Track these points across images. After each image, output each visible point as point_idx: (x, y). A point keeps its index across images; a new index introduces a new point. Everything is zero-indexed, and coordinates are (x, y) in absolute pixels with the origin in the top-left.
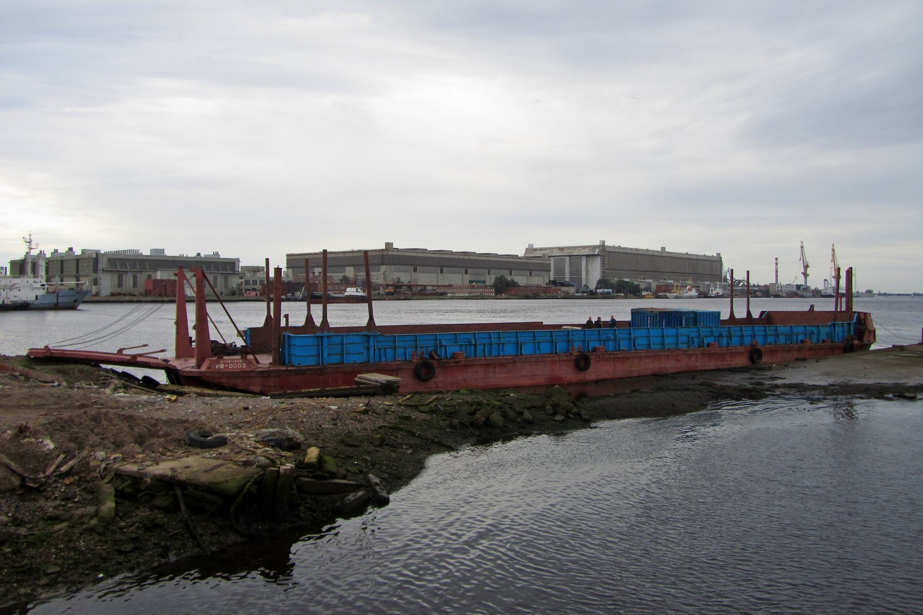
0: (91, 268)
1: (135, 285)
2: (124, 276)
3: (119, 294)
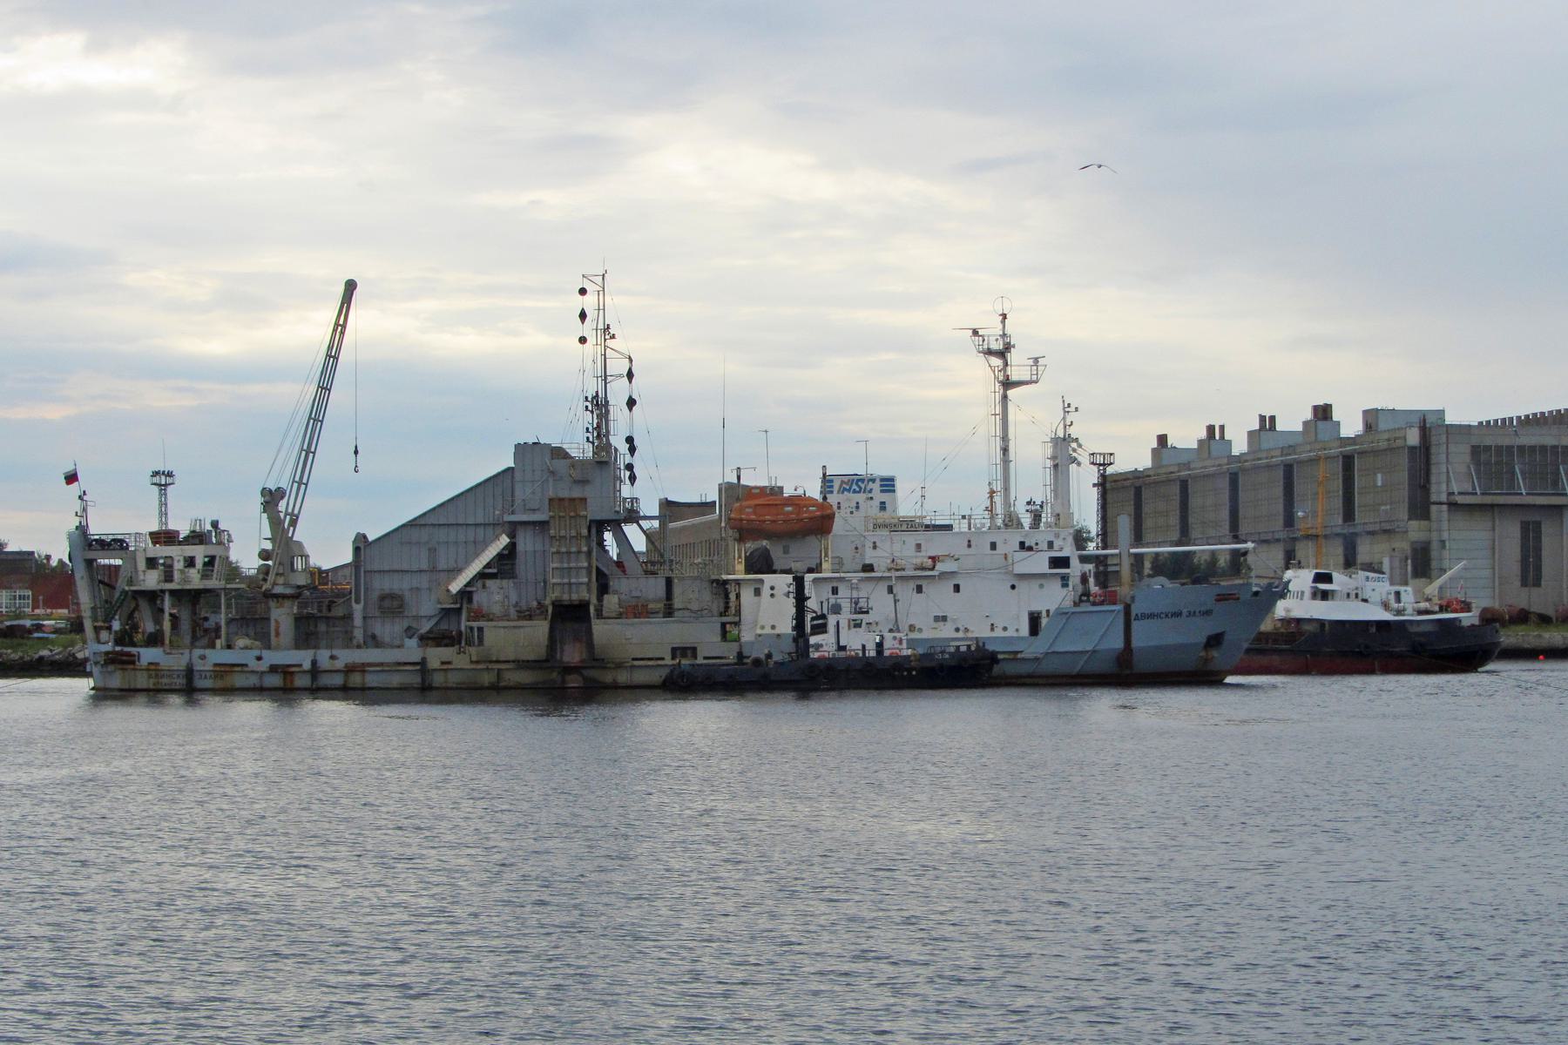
0: (1403, 493)
2: (1547, 529)
3: (1522, 617)
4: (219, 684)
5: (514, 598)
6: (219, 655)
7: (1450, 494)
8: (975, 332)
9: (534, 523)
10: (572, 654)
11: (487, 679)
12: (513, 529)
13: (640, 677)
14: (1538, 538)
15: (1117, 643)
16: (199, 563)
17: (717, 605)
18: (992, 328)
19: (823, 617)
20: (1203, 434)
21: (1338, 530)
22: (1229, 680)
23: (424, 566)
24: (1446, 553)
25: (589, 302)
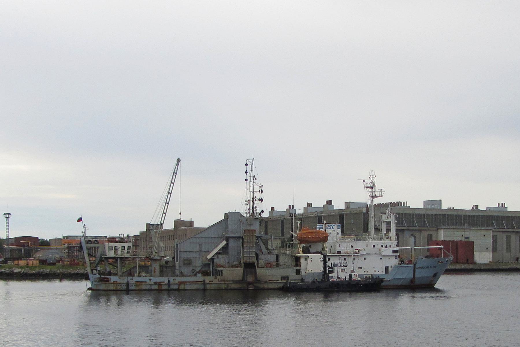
4: (137, 288)
5: (227, 260)
6: (136, 279)
8: (364, 181)
9: (235, 237)
10: (250, 279)
11: (224, 287)
12: (227, 239)
13: (271, 286)
15: (411, 276)
16: (126, 248)
17: (294, 263)
18: (368, 181)
19: (331, 268)
23: (198, 250)
25: (248, 168)
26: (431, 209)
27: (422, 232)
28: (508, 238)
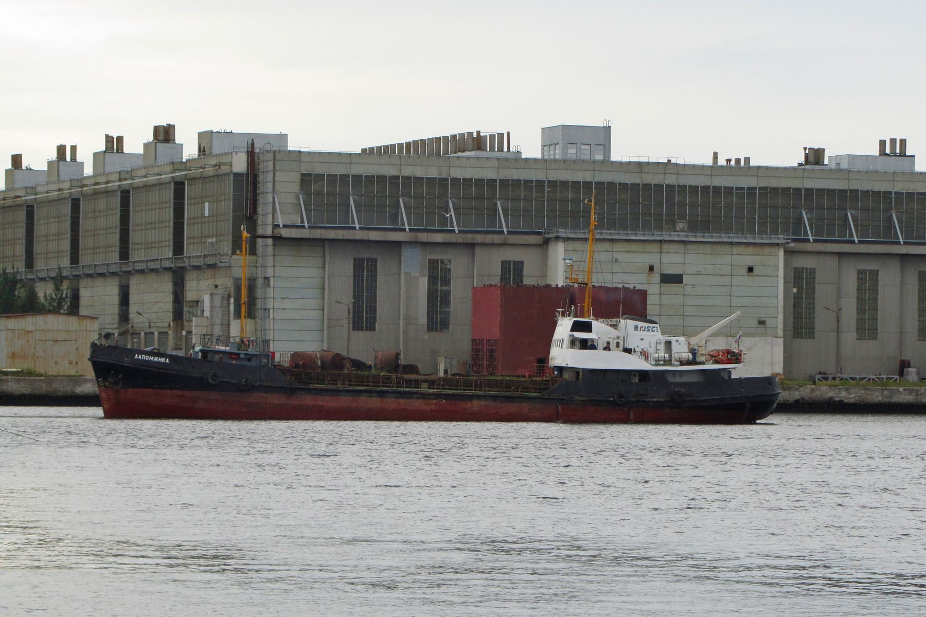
1: (438, 320)
7: (276, 226)
14: (373, 277)
20: (53, 156)
21: (167, 264)
22: (758, 421)
24: (270, 292)
26: (565, 162)
27: (478, 251)
28: (868, 285)
